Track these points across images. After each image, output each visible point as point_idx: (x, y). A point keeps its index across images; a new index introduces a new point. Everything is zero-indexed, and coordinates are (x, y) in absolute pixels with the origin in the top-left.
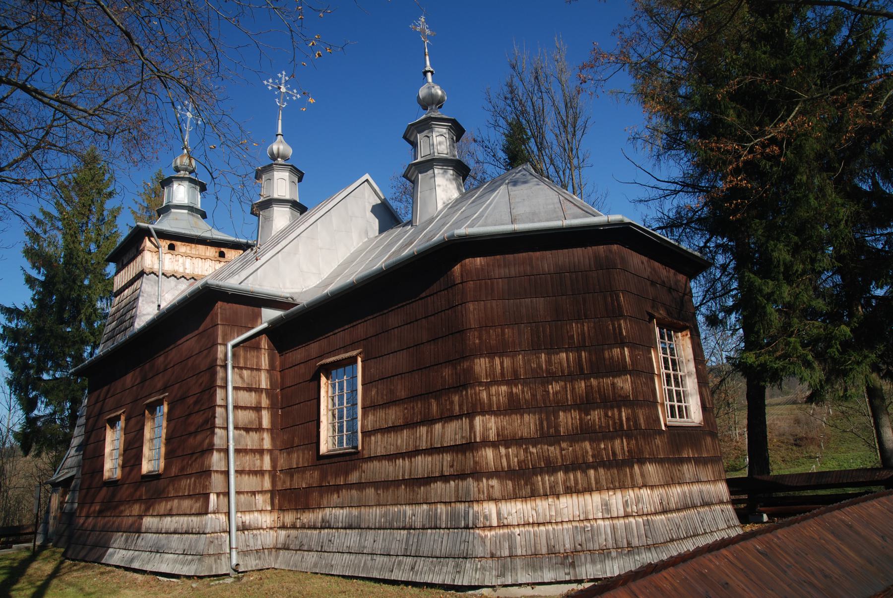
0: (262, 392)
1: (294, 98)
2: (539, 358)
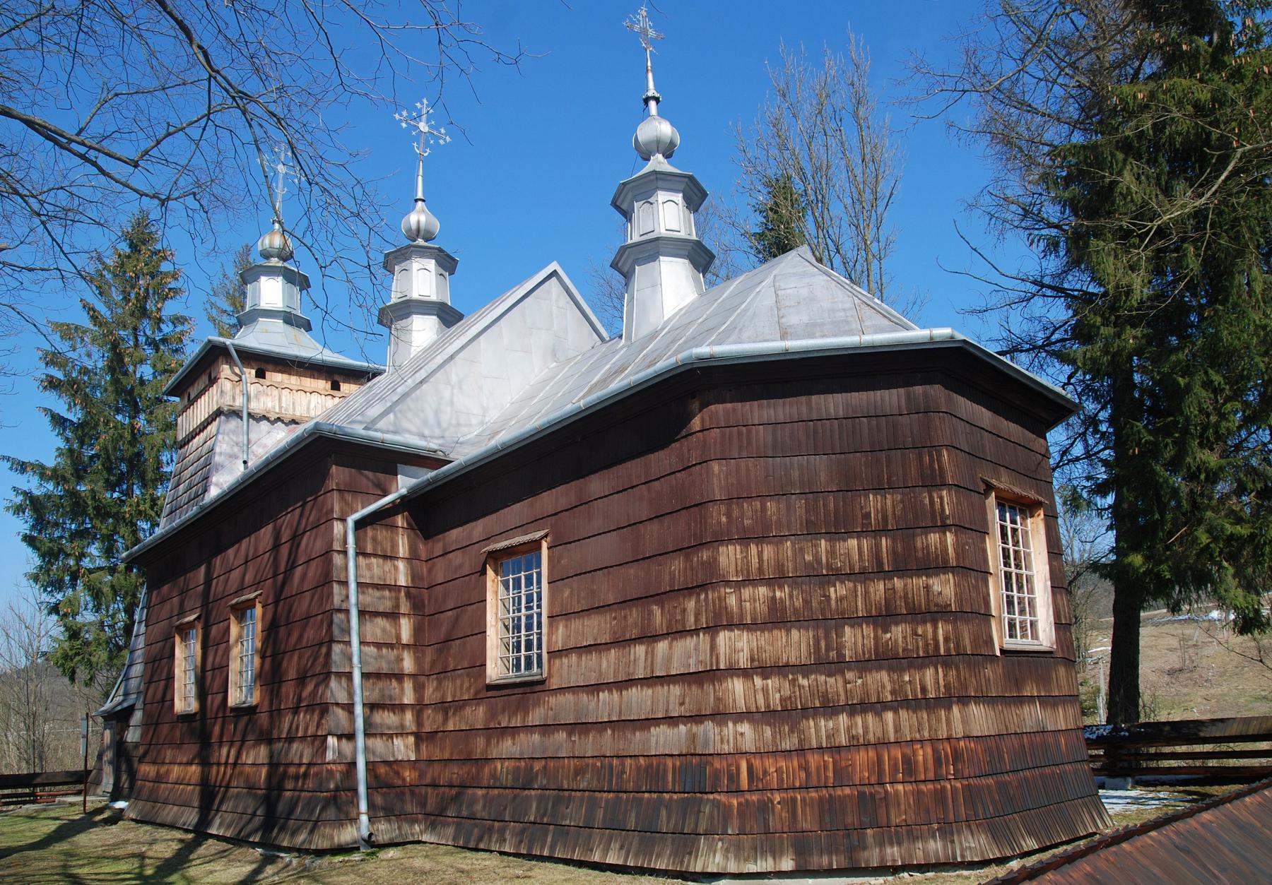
2: (816, 546)
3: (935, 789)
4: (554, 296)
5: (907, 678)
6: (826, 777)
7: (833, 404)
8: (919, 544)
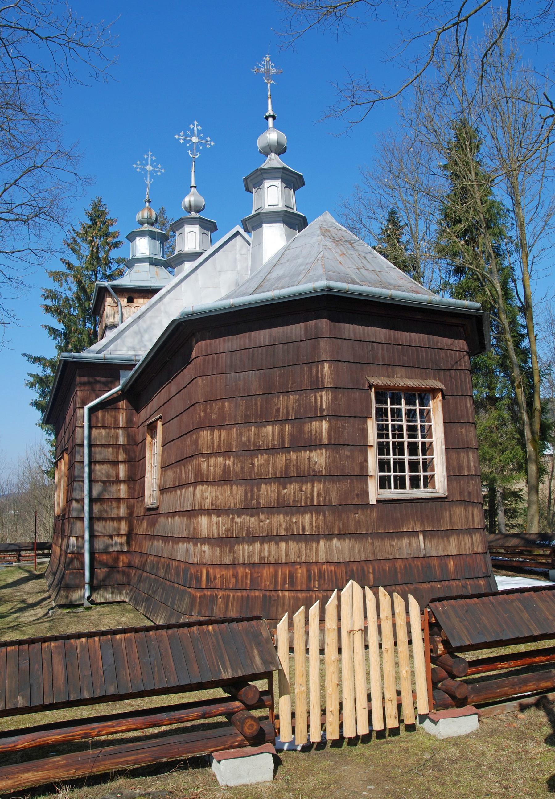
0: (119, 448)
1: (208, 146)
2: (249, 431)
3: (307, 597)
4: (238, 248)
5: (294, 520)
6: (246, 583)
7: (263, 336)
8: (306, 429)
